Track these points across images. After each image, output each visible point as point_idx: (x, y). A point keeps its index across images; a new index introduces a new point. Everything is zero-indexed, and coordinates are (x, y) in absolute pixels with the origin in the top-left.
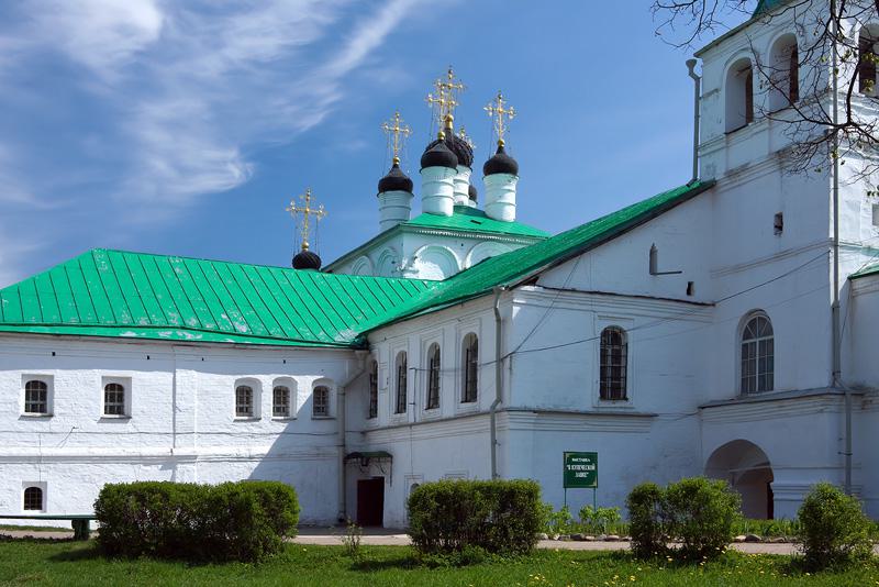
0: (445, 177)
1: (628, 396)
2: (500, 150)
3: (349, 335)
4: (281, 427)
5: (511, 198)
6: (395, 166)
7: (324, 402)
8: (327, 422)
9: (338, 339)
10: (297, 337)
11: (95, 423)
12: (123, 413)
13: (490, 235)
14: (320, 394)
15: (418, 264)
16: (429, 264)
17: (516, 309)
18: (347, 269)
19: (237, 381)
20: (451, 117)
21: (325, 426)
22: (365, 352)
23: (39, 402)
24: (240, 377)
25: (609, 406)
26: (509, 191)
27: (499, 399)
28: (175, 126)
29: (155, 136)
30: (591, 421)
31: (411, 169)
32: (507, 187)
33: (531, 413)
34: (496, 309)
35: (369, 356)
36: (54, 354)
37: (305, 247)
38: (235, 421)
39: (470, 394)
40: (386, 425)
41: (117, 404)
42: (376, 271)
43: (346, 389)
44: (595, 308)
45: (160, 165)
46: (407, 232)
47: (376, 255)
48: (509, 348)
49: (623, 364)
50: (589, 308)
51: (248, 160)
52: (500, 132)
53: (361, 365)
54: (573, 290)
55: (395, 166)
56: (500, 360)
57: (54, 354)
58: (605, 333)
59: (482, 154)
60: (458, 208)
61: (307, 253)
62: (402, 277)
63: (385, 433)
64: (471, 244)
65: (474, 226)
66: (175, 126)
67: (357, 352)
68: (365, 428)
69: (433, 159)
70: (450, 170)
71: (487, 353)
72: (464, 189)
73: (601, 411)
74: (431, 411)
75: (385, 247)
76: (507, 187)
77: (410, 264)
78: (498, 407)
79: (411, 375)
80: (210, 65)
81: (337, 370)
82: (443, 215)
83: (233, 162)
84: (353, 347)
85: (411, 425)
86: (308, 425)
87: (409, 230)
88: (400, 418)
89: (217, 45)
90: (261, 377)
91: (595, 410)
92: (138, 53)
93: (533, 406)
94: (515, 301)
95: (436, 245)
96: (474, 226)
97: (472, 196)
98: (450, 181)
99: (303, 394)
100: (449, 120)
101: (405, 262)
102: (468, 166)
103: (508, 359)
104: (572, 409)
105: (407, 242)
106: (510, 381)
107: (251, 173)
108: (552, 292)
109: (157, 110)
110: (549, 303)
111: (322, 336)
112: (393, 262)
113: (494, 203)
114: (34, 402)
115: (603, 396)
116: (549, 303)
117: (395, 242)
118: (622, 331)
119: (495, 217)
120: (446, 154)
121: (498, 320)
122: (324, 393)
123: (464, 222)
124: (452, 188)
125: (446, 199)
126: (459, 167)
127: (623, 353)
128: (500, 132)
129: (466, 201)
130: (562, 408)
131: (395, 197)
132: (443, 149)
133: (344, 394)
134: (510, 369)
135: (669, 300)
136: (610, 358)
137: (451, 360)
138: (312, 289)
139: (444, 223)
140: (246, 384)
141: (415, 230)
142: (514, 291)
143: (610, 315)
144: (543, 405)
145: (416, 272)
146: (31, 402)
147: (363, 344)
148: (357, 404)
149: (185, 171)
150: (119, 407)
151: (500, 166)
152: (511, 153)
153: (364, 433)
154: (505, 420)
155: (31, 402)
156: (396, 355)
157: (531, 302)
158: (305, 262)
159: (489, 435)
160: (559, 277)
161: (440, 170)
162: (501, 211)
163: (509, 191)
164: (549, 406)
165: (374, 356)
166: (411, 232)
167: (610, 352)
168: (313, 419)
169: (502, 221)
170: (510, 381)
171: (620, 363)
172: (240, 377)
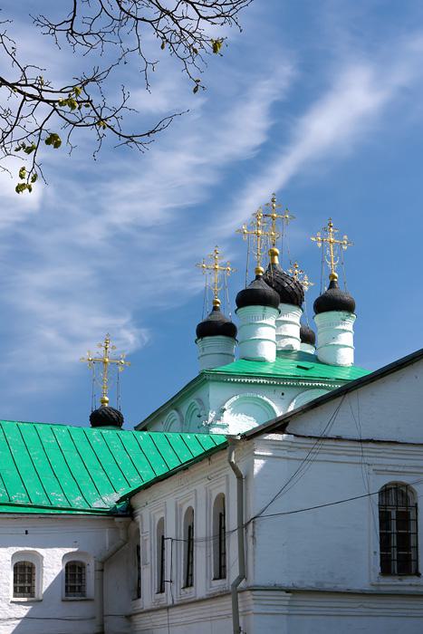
0: (263, 317)
1: (420, 571)
2: (332, 285)
3: (109, 500)
4: (23, 611)
5: (347, 339)
6: (215, 309)
7: (81, 580)
8: (83, 604)
9: (97, 504)
10: (45, 503)
11: (4, 605)
12: (32, 595)
13: (315, 381)
14: (73, 571)
15: (227, 417)
16: (242, 417)
17: (259, 464)
18: (160, 426)
19: (66, 556)
20: (277, 250)
21: (80, 609)
22: (128, 519)
23: (27, 584)
24: (21, 549)
25: (392, 583)
26: (344, 331)
27: (243, 576)
28: (60, 294)
29: (32, 303)
30: (373, 603)
31: (229, 313)
32: (341, 327)
33: (284, 593)
34: (231, 463)
35: (132, 525)
36: (27, 532)
37: (104, 402)
38: (12, 602)
39: (221, 573)
40: (149, 608)
41: (27, 584)
42: (185, 428)
43: (104, 564)
44: (370, 460)
45: (50, 335)
46: (213, 381)
47: (185, 408)
48: (252, 511)
49: (413, 530)
50: (358, 459)
51: (139, 326)
52: (333, 265)
53: (122, 535)
54: (338, 439)
55: (215, 309)
56: (242, 526)
57: (27, 532)
58: (385, 492)
59: (311, 288)
60: (284, 353)
61: (105, 408)
62: (208, 433)
63: (153, 615)
64: (295, 391)
65: (302, 373)
66: (60, 294)
67: (117, 520)
68: (130, 611)
69: (248, 298)
70: (270, 310)
71: (232, 522)
72: (294, 331)
73: (383, 589)
74: (187, 590)
75: (192, 400)
76: (341, 327)
77: (218, 418)
78: (242, 584)
79: (168, 543)
80: (92, 232)
81: (96, 541)
82: (263, 361)
83: (126, 327)
84: (112, 514)
85: (168, 608)
86: (58, 608)
87: (215, 378)
88: (159, 600)
89: (98, 211)
90: (41, 551)
91: (374, 589)
92: (18, 224)
93: (286, 582)
94: (256, 453)
95: (248, 395)
96: (302, 373)
97: (307, 337)
98: (271, 321)
99: (50, 571)
100: (274, 254)
101: (212, 415)
102: (300, 307)
103: (251, 525)
104: (342, 587)
105: (214, 392)
106: (254, 554)
107: (146, 339)
108: (309, 441)
109: (40, 278)
110: (303, 455)
111: (77, 502)
112: (199, 416)
113: (327, 345)
114: (22, 585)
115: (386, 570)
116: (303, 455)
117: (201, 393)
118: (407, 486)
119: (329, 362)
120: (274, 292)
121: (240, 477)
122: (80, 569)
123: (289, 368)
124: (273, 334)
125: (263, 342)
126: (282, 306)
127: (412, 516)
128: (333, 265)
129: (297, 345)
130: (327, 586)
131: (215, 343)
132: (262, 286)
133: (102, 570)
134: (253, 537)
135: (310, 437)
136: (394, 524)
137: (203, 528)
138: (84, 448)
139: (266, 370)
140: (76, 559)
141: (223, 378)
142: (255, 440)
143: (390, 468)
144: (301, 582)
145: (224, 427)
146: (18, 585)
147: (126, 511)
148: (116, 578)
149: (75, 340)
150: (29, 588)
151: (329, 304)
152: (345, 291)
153: (129, 617)
154: (247, 600)
155: (18, 585)
156: (157, 522)
157: (280, 453)
158: (104, 419)
159: (231, 621)
160: (314, 424)
161: (258, 310)
162: (335, 353)
163: (344, 331)
164: (310, 583)
165: (138, 524)
166: (217, 381)
167: (394, 515)
168: (63, 601)
169: (337, 366)
170: (254, 554)
171: (409, 529)
172: (21, 549)
